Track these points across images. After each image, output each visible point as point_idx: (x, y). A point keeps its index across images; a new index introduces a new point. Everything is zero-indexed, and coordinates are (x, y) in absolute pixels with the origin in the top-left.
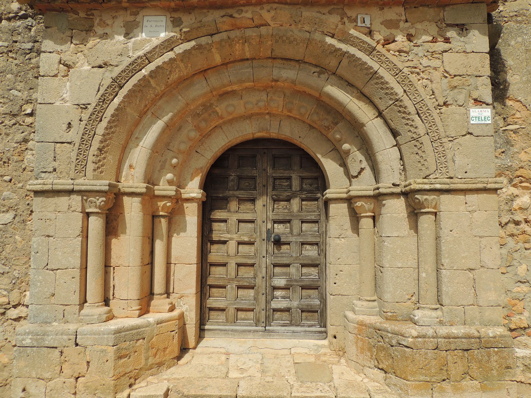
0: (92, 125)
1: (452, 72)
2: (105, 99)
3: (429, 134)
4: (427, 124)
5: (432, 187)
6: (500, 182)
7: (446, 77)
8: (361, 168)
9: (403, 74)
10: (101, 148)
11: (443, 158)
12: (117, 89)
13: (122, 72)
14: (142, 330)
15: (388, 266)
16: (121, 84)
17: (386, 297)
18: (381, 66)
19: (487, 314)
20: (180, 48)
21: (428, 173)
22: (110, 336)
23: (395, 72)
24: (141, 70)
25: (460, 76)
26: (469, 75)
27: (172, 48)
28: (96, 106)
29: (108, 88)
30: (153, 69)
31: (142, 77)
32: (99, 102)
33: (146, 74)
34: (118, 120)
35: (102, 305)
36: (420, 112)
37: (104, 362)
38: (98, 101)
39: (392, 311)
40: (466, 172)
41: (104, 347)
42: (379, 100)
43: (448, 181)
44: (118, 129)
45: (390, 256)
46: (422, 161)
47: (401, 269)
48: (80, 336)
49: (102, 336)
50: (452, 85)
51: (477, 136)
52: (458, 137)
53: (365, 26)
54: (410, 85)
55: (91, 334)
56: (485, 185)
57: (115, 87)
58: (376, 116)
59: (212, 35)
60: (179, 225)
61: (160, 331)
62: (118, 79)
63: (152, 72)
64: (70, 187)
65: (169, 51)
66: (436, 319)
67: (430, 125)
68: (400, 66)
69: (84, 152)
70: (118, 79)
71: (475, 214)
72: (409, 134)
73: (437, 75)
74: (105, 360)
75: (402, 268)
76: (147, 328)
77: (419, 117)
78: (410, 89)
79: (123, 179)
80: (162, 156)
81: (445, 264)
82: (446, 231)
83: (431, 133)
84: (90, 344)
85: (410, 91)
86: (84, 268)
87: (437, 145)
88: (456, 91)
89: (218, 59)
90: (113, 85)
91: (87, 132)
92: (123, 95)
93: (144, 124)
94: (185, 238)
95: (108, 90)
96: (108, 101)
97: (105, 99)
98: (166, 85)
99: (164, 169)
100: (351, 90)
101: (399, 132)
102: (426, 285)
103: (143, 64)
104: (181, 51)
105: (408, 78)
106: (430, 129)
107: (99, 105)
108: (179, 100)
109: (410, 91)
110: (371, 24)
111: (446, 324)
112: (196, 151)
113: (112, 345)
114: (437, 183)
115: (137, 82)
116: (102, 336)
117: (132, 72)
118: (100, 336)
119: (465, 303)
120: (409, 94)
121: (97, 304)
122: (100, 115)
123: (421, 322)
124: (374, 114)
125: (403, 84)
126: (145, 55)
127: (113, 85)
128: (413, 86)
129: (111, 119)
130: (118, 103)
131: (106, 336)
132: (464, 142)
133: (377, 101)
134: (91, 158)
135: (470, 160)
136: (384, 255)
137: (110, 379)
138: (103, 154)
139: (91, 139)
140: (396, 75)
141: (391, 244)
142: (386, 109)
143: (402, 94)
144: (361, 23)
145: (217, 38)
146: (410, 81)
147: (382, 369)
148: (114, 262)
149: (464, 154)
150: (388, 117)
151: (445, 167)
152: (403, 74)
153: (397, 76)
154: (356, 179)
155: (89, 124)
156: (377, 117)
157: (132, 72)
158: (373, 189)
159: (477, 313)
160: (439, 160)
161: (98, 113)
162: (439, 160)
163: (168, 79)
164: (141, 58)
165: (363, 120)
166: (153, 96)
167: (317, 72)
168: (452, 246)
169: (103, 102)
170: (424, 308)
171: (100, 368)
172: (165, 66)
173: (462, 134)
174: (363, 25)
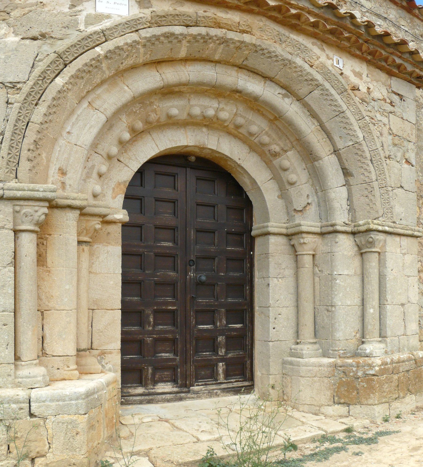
1: (394, 131)
2: (45, 78)
3: (378, 180)
4: (377, 172)
7: (391, 134)
8: (308, 204)
9: (365, 122)
11: (387, 205)
13: (72, 46)
15: (340, 304)
16: (67, 61)
17: (338, 336)
18: (348, 107)
20: (147, 32)
21: (377, 216)
22: (80, 401)
23: (359, 117)
24: (93, 48)
25: (399, 136)
26: (404, 138)
27: (137, 29)
28: (34, 84)
29: (51, 63)
30: (111, 49)
31: (96, 56)
32: (38, 80)
33: (102, 53)
36: (373, 159)
37: (73, 436)
38: (36, 78)
39: (343, 349)
41: (73, 416)
42: (339, 138)
43: (392, 224)
45: (341, 294)
46: (371, 204)
47: (350, 307)
48: (37, 404)
49: (68, 402)
54: (369, 132)
55: (52, 400)
57: (60, 64)
58: (331, 152)
59: (187, 26)
60: (98, 258)
62: (65, 54)
65: (132, 32)
67: (379, 173)
68: (364, 113)
70: (65, 54)
71: (406, 256)
72: (362, 177)
73: (385, 130)
74: (75, 434)
77: (372, 163)
78: (368, 136)
80: (88, 161)
81: (389, 300)
83: (380, 180)
84: (52, 414)
85: (368, 138)
87: (383, 192)
89: (183, 53)
90: (57, 61)
92: (69, 75)
93: (78, 116)
94: (106, 275)
95: (51, 66)
96: (48, 79)
97: (45, 78)
99: (91, 178)
100: (311, 121)
101: (352, 173)
102: (374, 320)
103: (98, 40)
105: (369, 126)
106: (380, 177)
107: (38, 83)
108: (125, 91)
109: (368, 138)
110: (343, 67)
112: (118, 160)
113: (83, 413)
114: (386, 226)
115: (89, 61)
116: (68, 402)
117: (83, 49)
118: (66, 403)
120: (366, 140)
123: (374, 353)
124: (329, 151)
125: (363, 130)
126: (103, 31)
127: (57, 61)
128: (371, 135)
130: (62, 84)
131: (73, 402)
133: (336, 138)
135: (404, 209)
136: (336, 293)
137: (82, 457)
140: (360, 120)
141: (342, 282)
142: (343, 148)
143: (362, 139)
144: (337, 64)
146: (370, 129)
147: (344, 403)
150: (344, 156)
151: (390, 212)
152: (365, 122)
153: (360, 121)
154: (300, 214)
155: (24, 108)
156: (331, 154)
158: (320, 226)
160: (384, 206)
162: (384, 206)
163: (122, 63)
164: (98, 34)
165: (321, 154)
167: (282, 95)
169: (42, 80)
170: (372, 341)
171: (68, 444)
174: (338, 66)
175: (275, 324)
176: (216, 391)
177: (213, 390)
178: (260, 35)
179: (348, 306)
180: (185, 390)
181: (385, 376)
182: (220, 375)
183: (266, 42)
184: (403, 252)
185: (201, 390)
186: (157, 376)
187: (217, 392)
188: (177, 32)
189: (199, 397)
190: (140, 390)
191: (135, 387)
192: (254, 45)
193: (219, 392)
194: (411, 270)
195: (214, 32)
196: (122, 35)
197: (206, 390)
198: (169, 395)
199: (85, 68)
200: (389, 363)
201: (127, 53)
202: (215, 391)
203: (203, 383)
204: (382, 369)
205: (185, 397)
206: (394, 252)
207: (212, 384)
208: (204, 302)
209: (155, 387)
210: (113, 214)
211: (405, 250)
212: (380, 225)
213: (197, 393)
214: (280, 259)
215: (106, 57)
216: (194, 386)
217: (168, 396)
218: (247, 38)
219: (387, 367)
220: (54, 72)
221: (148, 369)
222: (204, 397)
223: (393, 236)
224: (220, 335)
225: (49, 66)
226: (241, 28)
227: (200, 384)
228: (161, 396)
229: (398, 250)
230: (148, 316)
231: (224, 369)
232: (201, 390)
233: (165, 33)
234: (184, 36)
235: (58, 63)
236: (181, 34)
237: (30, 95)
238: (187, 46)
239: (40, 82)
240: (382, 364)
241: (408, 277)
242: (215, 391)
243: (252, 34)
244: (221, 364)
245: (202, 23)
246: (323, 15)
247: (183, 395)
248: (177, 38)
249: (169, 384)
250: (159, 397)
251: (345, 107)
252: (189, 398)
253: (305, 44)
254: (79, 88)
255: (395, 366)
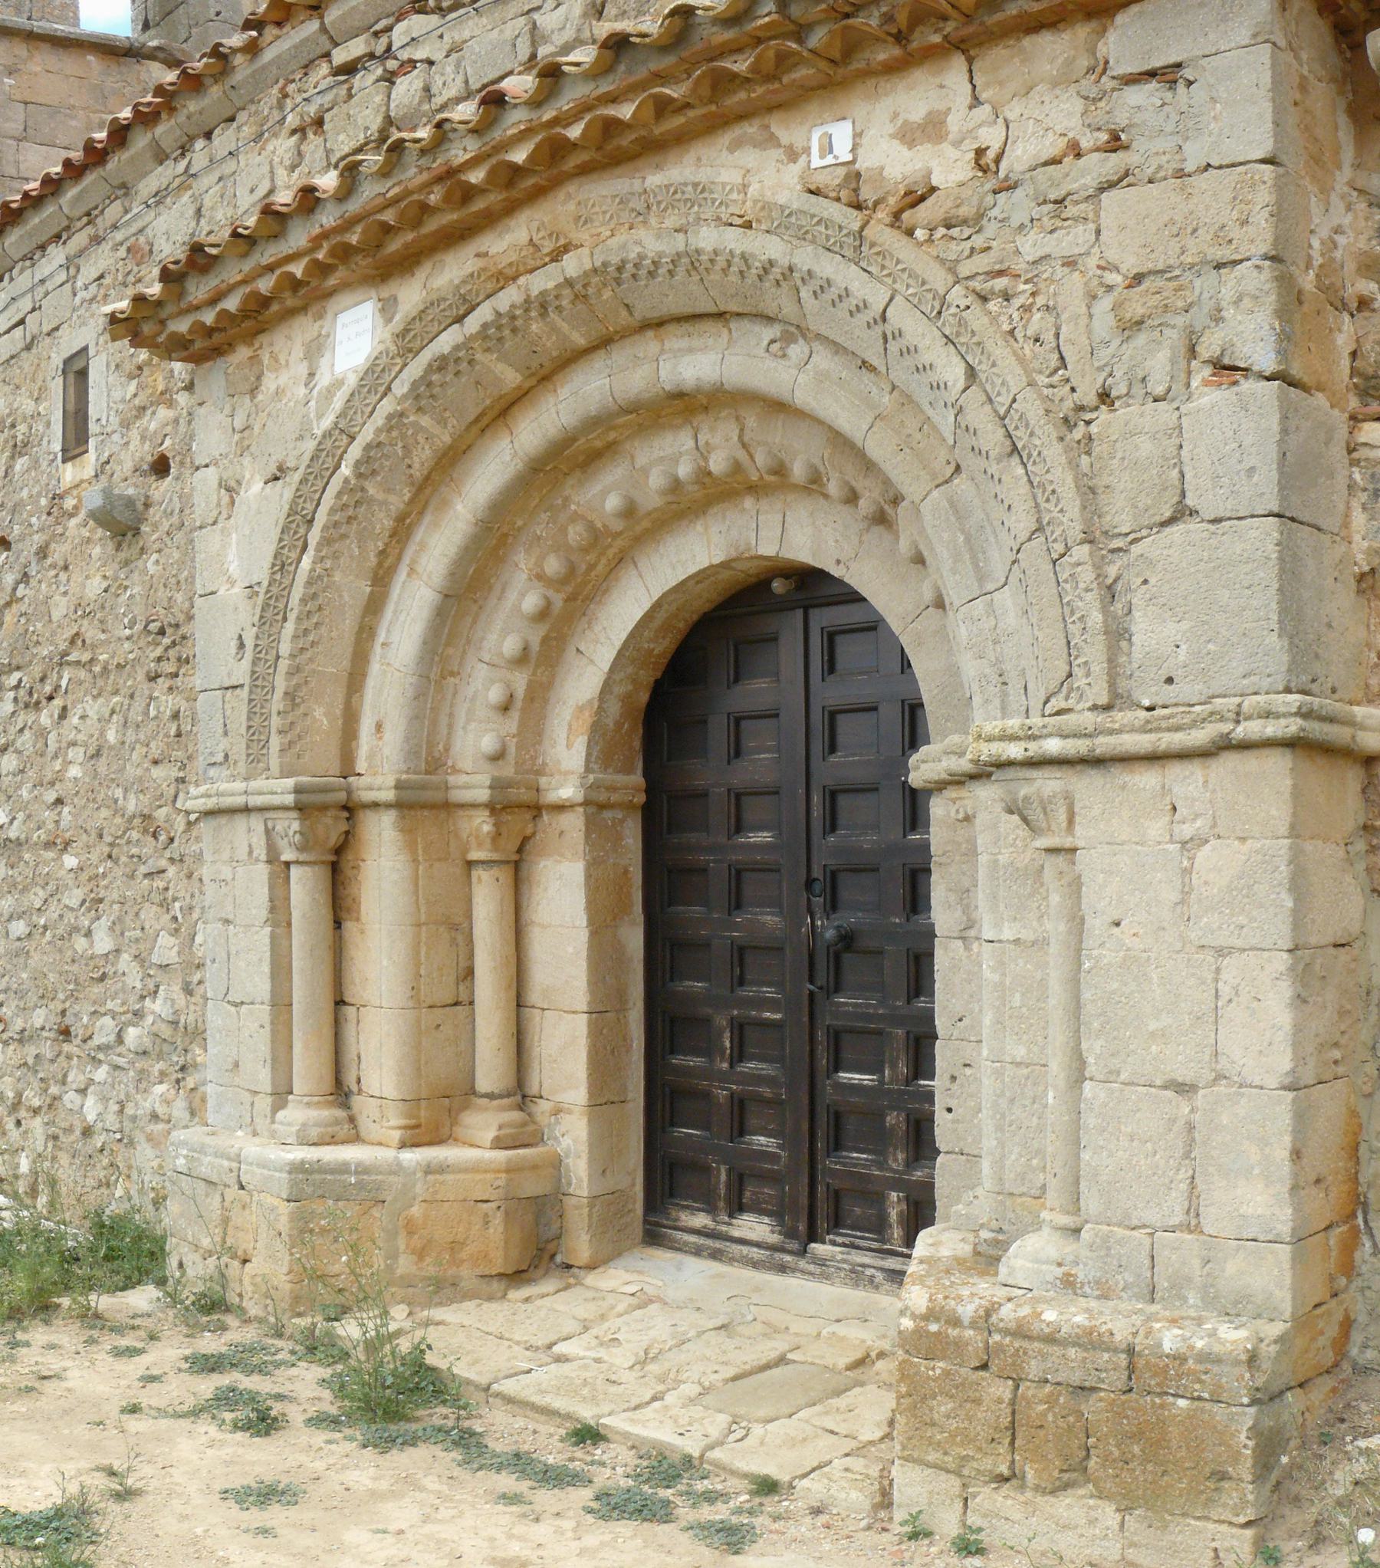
0: (270, 636)
2: (283, 566)
5: (1034, 749)
6: (1282, 709)
10: (291, 690)
12: (302, 531)
14: (373, 1177)
19: (1231, 1268)
34: (320, 609)
35: (319, 1103)
40: (1170, 680)
44: (323, 630)
47: (1025, 1071)
50: (1128, 316)
51: (1216, 521)
52: (1144, 532)
53: (834, 162)
56: (1226, 727)
57: (298, 526)
59: (459, 320)
60: (546, 889)
61: (436, 1192)
63: (358, 464)
64: (239, 801)
66: (1053, 1268)
69: (262, 707)
71: (1203, 854)
75: (1028, 1066)
76: (392, 1178)
79: (361, 766)
82: (1097, 922)
86: (281, 1003)
88: (1141, 339)
91: (262, 656)
97: (283, 566)
98: (412, 484)
104: (405, 390)
111: (1087, 1289)
114: (1050, 735)
119: (1153, 1217)
121: (306, 1099)
122: (281, 606)
129: (301, 612)
132: (1165, 552)
134: (275, 722)
135: (1185, 625)
138: (298, 705)
139: (271, 671)
145: (473, 324)
148: (534, 997)
149: (1162, 600)
157: (322, 477)
159: (1196, 1263)
161: (277, 600)
166: (388, 523)
168: (1115, 985)
172: (383, 437)
173: (1158, 519)
174: (829, 160)
175: (952, 1097)
176: (873, 1271)
177: (863, 1266)
178: (592, 236)
179: (1018, 1064)
180: (794, 1245)
181: (941, 1364)
182: (891, 1226)
183: (613, 243)
184: (1187, 831)
185: (833, 1257)
186: (747, 1194)
187: (873, 1276)
188: (446, 350)
189: (825, 1277)
190: (701, 1220)
191: (694, 1210)
192: (595, 270)
193: (880, 1276)
194: (1242, 919)
195: (509, 298)
196: (372, 413)
197: (844, 1261)
198: (755, 1250)
199: (336, 518)
200: (966, 1323)
201: (400, 445)
202: (869, 1272)
203: (847, 1240)
204: (928, 1332)
205: (792, 1265)
206: (1124, 837)
207: (870, 1250)
208: (851, 1004)
209: (734, 1221)
210: (557, 789)
211: (1199, 823)
212: (1014, 738)
213: (822, 1262)
214: (964, 874)
215: (360, 476)
216: (824, 1242)
217: (755, 1253)
218: (572, 265)
219: (953, 1332)
220: (295, 546)
221: (719, 1170)
222: (837, 1280)
223: (1116, 770)
224: (892, 1108)
225: (281, 540)
226: (546, 250)
227: (839, 1240)
228: (740, 1247)
229: (1156, 828)
230: (720, 1035)
231: (902, 1212)
232: (833, 1257)
233: (430, 365)
234: (467, 345)
235: (294, 526)
236: (457, 348)
237: (268, 605)
238: (497, 359)
239: (278, 577)
240: (930, 1315)
241: (1221, 952)
242: (869, 1272)
243: (577, 247)
244: (894, 1195)
245: (477, 295)
246: (632, 79)
247: (788, 1258)
248: (457, 360)
249: (766, 1220)
250: (736, 1249)
251: (877, 296)
252: (802, 1272)
253: (692, 179)
254: (351, 557)
255: (999, 1345)
